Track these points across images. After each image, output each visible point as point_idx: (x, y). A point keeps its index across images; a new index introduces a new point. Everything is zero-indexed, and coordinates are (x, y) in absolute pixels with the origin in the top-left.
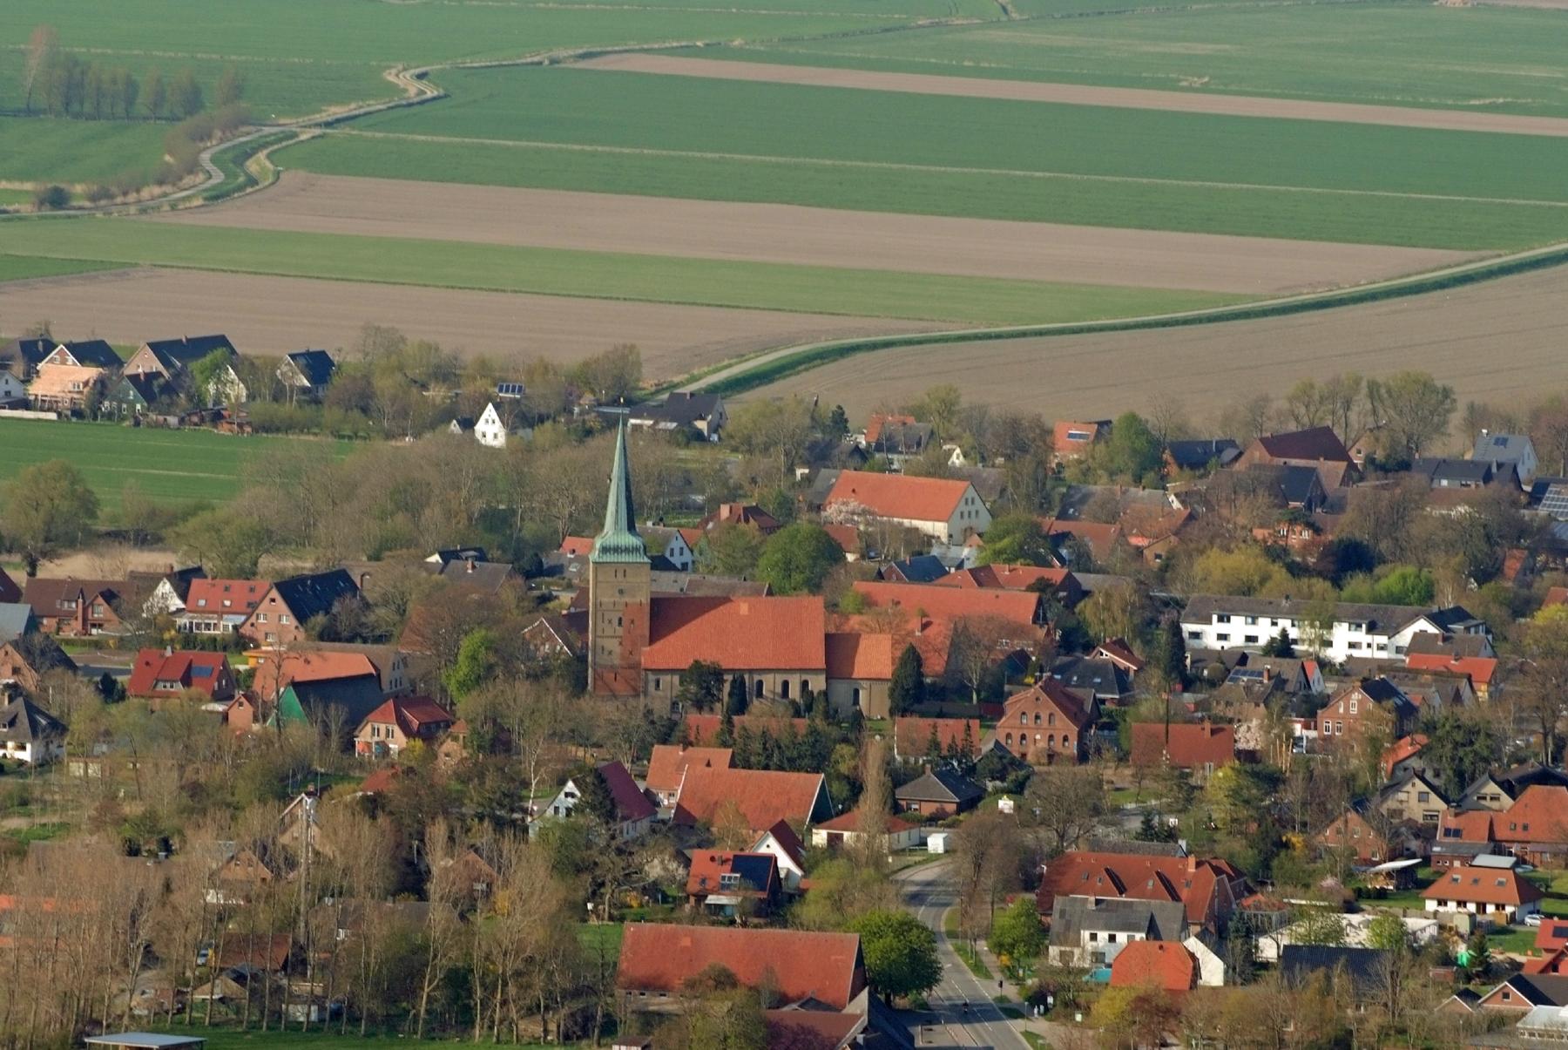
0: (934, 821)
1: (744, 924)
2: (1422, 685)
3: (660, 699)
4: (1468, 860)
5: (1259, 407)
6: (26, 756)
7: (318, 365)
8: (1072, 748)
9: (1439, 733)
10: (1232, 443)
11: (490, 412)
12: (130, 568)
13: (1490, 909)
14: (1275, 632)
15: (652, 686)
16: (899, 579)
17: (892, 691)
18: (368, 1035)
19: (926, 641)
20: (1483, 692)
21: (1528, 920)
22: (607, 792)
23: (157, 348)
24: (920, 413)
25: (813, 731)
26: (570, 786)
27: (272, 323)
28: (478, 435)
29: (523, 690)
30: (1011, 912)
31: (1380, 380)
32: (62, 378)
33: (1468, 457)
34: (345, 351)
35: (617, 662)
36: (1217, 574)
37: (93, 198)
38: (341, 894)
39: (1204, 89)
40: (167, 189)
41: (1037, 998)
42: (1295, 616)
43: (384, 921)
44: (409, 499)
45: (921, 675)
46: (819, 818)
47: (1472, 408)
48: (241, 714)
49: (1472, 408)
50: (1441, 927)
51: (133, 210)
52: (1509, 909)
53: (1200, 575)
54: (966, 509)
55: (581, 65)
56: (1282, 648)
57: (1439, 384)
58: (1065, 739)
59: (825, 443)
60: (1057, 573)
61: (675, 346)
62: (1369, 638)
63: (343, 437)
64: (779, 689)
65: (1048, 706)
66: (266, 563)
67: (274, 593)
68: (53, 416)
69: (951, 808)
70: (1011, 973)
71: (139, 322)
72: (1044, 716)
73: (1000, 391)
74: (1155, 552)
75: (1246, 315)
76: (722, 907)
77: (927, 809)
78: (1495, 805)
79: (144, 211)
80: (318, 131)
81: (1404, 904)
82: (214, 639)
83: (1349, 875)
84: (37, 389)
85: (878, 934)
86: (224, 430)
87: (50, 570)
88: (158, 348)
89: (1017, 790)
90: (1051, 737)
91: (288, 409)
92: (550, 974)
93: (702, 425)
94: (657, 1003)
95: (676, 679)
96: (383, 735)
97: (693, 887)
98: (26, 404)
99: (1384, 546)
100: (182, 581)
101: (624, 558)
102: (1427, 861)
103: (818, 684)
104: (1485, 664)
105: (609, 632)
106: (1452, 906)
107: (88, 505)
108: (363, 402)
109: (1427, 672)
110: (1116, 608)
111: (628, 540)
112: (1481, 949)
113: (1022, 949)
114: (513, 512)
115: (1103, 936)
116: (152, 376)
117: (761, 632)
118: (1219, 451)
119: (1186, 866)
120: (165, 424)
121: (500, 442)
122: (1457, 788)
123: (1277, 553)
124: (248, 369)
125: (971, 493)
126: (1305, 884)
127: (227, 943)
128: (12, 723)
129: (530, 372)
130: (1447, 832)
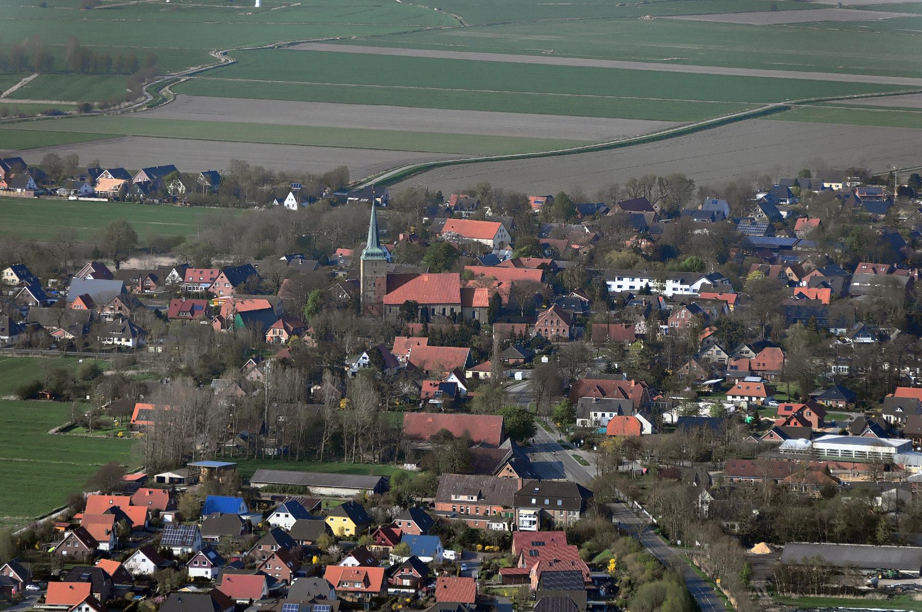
0: (516, 366)
1: (445, 412)
2: (708, 305)
3: (392, 317)
4: (741, 379)
5: (614, 189)
6: (130, 344)
7: (214, 177)
8: (567, 334)
10: (603, 204)
11: (291, 195)
12: (157, 264)
13: (754, 399)
14: (643, 284)
15: (388, 312)
16: (480, 265)
18: (299, 461)
19: (502, 290)
20: (732, 308)
21: (770, 403)
22: (382, 357)
23: (146, 171)
24: (472, 194)
25: (462, 330)
26: (365, 355)
27: (195, 159)
29: (337, 314)
30: (559, 406)
32: (108, 184)
33: (700, 207)
34: (224, 169)
35: (373, 301)
36: (615, 260)
37: (101, 107)
39: (552, 55)
40: (131, 103)
41: (576, 441)
43: (303, 412)
44: (269, 233)
45: (501, 305)
46: (469, 366)
47: (701, 188)
48: (217, 325)
49: (701, 188)
50: (737, 408)
51: (119, 112)
53: (608, 261)
55: (291, 48)
56: (646, 291)
57: (688, 178)
59: (434, 207)
60: (548, 261)
61: (364, 167)
62: (682, 286)
65: (556, 318)
66: (214, 262)
67: (222, 274)
68: (106, 200)
70: (562, 430)
71: (140, 158)
72: (555, 321)
73: (505, 183)
74: (585, 250)
75: (592, 150)
77: (512, 361)
79: (123, 112)
80: (188, 78)
81: (719, 398)
82: (197, 293)
83: (694, 387)
84: (98, 189)
85: (510, 416)
86: (178, 205)
87: (124, 266)
88: (148, 171)
89: (548, 353)
91: (204, 195)
92: (376, 434)
93: (379, 200)
94: (422, 445)
96: (278, 333)
97: (423, 396)
98: (94, 195)
99: (681, 248)
100: (182, 269)
101: (376, 258)
102: (724, 380)
104: (731, 297)
105: (370, 289)
106: (738, 398)
107: (133, 237)
108: (236, 193)
109: (709, 300)
110: (576, 277)
112: (756, 416)
114: (310, 238)
115: (599, 414)
116: (146, 183)
117: (432, 288)
120: (153, 203)
121: (295, 208)
122: (731, 348)
123: (637, 250)
124: (188, 179)
125: (503, 227)
126: (677, 392)
127: (240, 422)
128: (123, 331)
129: (303, 178)
130: (732, 367)
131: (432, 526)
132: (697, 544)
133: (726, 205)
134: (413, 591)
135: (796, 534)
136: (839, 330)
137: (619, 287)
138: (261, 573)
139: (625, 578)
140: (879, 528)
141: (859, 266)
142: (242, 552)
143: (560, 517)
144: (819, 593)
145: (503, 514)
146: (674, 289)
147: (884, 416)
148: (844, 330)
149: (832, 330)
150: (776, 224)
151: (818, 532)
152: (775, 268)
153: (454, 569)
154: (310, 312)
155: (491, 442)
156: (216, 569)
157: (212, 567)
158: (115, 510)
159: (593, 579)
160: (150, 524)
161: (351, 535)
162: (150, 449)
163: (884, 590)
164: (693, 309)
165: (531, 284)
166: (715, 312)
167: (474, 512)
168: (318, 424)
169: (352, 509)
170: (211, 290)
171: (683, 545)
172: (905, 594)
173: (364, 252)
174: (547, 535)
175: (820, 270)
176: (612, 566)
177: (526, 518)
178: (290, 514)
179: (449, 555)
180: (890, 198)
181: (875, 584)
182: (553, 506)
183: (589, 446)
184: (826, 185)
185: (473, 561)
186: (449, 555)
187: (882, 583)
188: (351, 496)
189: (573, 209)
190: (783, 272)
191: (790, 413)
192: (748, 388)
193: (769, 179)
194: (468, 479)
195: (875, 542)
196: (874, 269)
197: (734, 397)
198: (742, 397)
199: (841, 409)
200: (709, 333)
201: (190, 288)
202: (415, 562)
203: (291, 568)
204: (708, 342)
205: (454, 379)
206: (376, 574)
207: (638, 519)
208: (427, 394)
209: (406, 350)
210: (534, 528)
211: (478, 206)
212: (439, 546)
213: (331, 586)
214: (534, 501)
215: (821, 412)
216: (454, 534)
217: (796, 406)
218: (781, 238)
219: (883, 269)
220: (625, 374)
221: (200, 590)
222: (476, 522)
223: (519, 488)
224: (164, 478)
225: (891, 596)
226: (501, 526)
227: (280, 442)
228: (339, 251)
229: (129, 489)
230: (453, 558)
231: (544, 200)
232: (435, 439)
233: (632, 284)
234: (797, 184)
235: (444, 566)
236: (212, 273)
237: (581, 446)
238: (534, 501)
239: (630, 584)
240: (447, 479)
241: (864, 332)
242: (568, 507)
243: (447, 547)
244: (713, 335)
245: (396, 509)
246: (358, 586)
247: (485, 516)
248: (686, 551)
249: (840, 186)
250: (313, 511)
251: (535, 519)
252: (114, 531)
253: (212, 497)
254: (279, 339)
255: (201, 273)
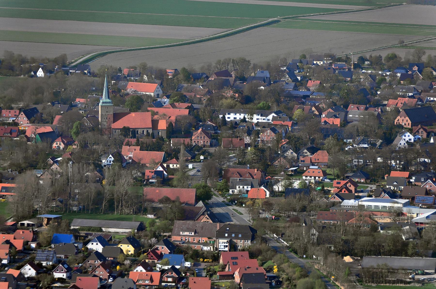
5: (209, 66)
9: (292, 139)
10: (205, 74)
11: (40, 70)
13: (317, 178)
17: (167, 132)
26: (111, 156)
28: (39, 76)
29: (90, 134)
30: (221, 183)
31: (235, 59)
38: (87, 181)
42: (245, 113)
46: (164, 161)
47: (254, 64)
49: (254, 64)
52: (321, 178)
54: (157, 90)
56: (244, 120)
58: (207, 142)
62: (261, 117)
63: (8, 76)
64: (142, 132)
67: (22, 113)
69: (190, 158)
70: (223, 196)
72: (203, 137)
73: (155, 64)
76: (153, 182)
78: (306, 154)
89: (203, 154)
90: (204, 142)
94: (155, 205)
95: (119, 131)
97: (146, 178)
103: (150, 131)
106: (308, 178)
108: (12, 68)
110: (206, 112)
111: (108, 100)
113: (225, 190)
115: (241, 187)
117: (136, 120)
118: (202, 75)
119: (254, 171)
122: (297, 150)
130: (302, 161)
131: (175, 249)
132: (314, 257)
133: (268, 74)
134: (174, 284)
135: (366, 251)
136: (349, 140)
137: (229, 118)
138: (95, 276)
139: (284, 276)
140: (410, 248)
141: (350, 106)
142: (78, 264)
143: (240, 244)
144: (386, 283)
145: (208, 242)
146: (257, 119)
147: (388, 187)
148: (351, 140)
149: (345, 141)
150: (298, 85)
151: (377, 251)
152: (307, 107)
153: (192, 272)
154: (74, 133)
155: (190, 202)
156: (68, 273)
157: (66, 272)
158: (7, 242)
159: (268, 277)
160: (25, 249)
161: (132, 254)
162: (15, 208)
163: (419, 281)
164: (273, 130)
165: (185, 117)
166: (283, 131)
167: (192, 241)
168: (99, 194)
169: (131, 240)
170: (16, 121)
171: (306, 257)
172: (429, 283)
173: (101, 101)
174: (234, 254)
175: (332, 109)
176: (276, 270)
177: (222, 244)
178: (99, 243)
179: (188, 264)
180: (349, 69)
181: (413, 278)
182: (237, 237)
183: (240, 204)
184: (315, 62)
185: (199, 267)
186: (188, 264)
187: (417, 277)
188: (125, 233)
189: (193, 77)
190: (311, 109)
191: (340, 186)
192: (313, 172)
193: (285, 59)
194: (189, 224)
195: (407, 255)
196: (357, 108)
197: (306, 177)
198: (311, 177)
199: (363, 183)
200: (284, 143)
201: (4, 120)
202: (173, 269)
203: (108, 273)
204: (284, 147)
205: (160, 169)
206: (156, 276)
207: (278, 244)
208: (148, 176)
209: (130, 153)
210: (227, 249)
211: (140, 75)
212: (183, 260)
213: (135, 283)
214: (226, 235)
215: (355, 184)
216: (187, 253)
217: (343, 182)
218: (302, 91)
219: (362, 107)
220: (248, 165)
221: (63, 285)
222: (195, 246)
223: (218, 228)
224: (24, 224)
225: (423, 284)
226: (209, 248)
227: (79, 204)
228: (78, 100)
229: (12, 229)
230: (189, 266)
231: (173, 71)
232: (161, 201)
233: (235, 116)
234: (301, 62)
235: (187, 270)
236: (15, 112)
237: (235, 204)
238: (226, 235)
239: (288, 279)
240: (178, 223)
241: (363, 142)
242: (244, 238)
243: (186, 260)
244: (287, 143)
245: (154, 240)
246: (147, 282)
247: (199, 243)
248: (309, 261)
249: (322, 63)
250: (109, 241)
251: (227, 245)
252: (10, 254)
253: (55, 234)
254: (59, 147)
255: (10, 112)
